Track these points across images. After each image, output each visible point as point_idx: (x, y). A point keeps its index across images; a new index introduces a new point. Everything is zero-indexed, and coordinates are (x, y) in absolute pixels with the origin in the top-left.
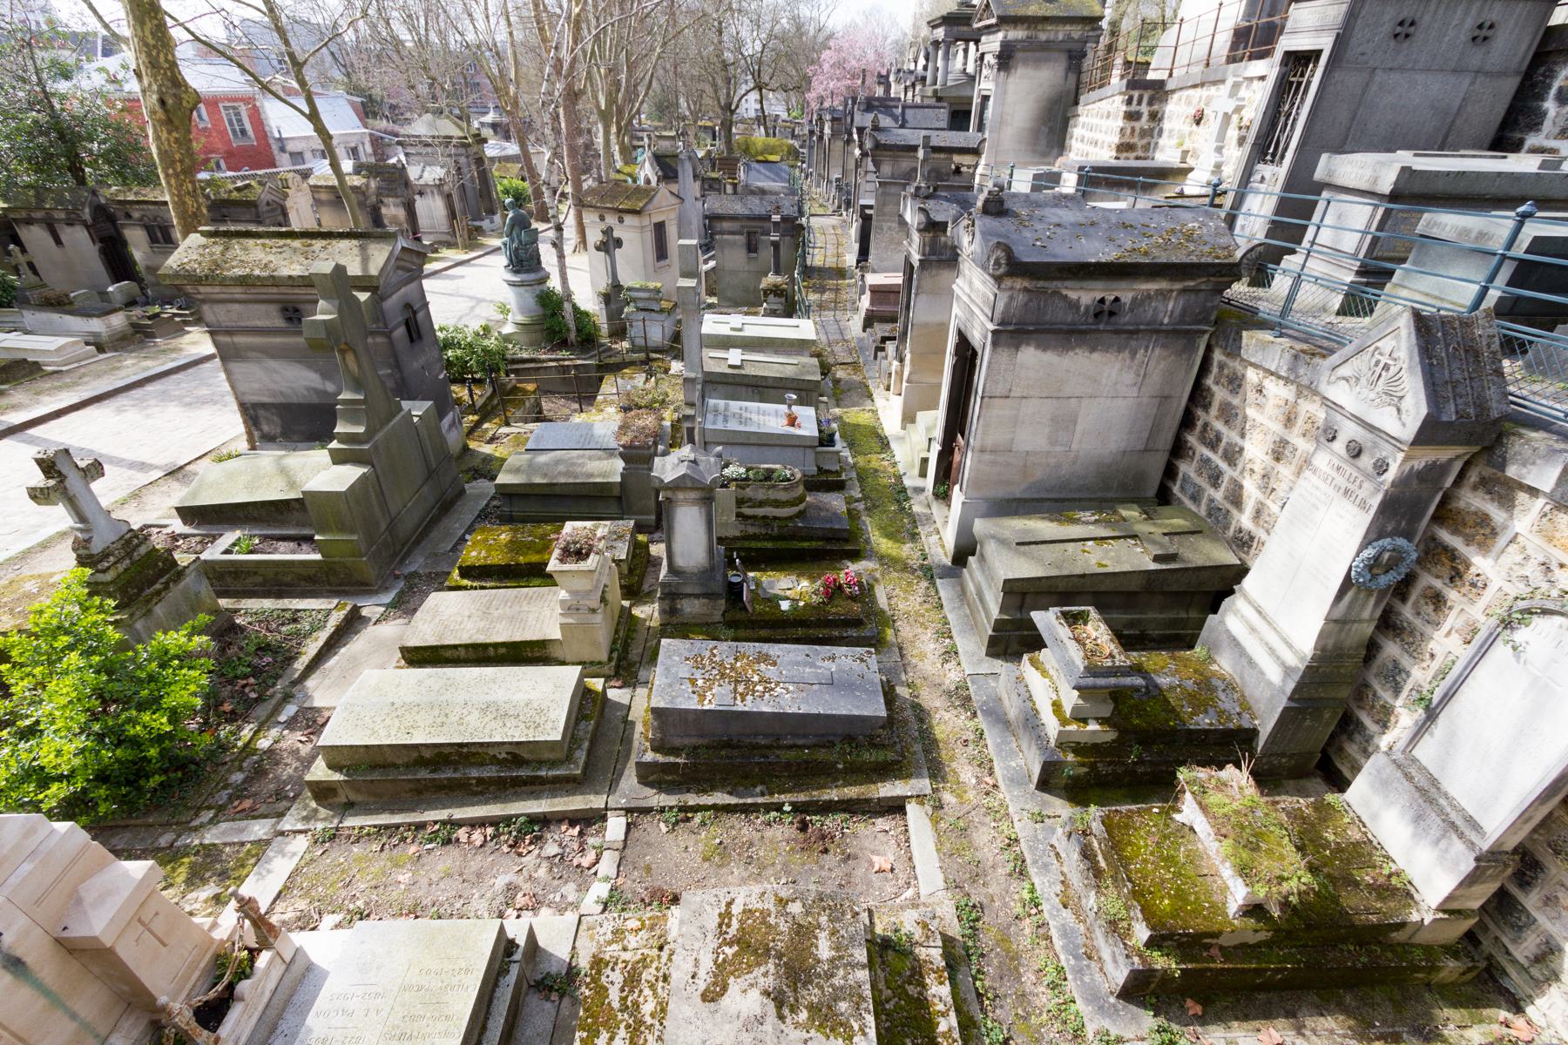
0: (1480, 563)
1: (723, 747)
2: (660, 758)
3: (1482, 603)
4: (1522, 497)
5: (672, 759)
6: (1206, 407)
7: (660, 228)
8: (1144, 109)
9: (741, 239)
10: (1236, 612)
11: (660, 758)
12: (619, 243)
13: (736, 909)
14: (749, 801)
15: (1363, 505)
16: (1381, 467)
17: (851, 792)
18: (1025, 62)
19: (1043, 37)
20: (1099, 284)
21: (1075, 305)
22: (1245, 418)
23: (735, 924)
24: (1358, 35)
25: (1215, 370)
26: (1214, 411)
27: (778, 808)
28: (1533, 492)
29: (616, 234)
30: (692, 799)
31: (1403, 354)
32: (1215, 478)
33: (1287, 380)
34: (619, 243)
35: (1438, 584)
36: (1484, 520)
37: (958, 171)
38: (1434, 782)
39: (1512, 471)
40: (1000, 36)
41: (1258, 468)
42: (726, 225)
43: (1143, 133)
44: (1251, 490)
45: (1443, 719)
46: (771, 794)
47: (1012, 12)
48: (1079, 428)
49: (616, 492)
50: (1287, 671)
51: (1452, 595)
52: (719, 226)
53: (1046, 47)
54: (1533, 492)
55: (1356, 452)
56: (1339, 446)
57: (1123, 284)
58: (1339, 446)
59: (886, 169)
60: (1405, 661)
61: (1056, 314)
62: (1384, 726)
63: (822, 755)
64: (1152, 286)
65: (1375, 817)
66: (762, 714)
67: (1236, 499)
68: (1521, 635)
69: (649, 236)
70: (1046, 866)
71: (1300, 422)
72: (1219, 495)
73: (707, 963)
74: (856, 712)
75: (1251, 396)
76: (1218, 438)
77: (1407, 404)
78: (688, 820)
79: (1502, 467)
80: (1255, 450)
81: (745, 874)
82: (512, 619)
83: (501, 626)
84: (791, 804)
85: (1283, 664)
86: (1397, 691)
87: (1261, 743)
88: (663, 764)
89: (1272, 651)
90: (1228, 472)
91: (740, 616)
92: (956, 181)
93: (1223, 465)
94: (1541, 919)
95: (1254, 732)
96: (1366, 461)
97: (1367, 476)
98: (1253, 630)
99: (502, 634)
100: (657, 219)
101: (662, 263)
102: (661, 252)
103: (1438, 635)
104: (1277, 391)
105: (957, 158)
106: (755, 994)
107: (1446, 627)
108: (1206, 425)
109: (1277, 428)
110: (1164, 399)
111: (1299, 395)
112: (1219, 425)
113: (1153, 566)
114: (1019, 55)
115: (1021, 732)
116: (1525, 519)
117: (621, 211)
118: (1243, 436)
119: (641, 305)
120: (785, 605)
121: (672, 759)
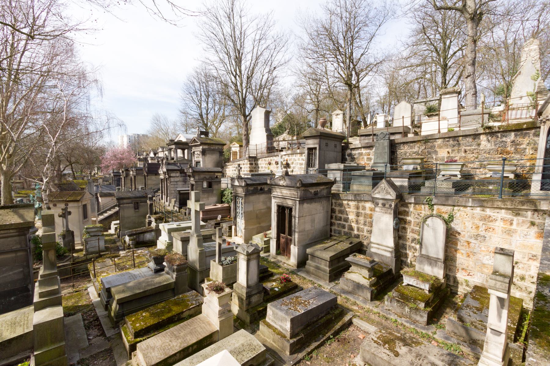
0: (409, 218)
1: (307, 327)
2: (295, 340)
3: (412, 225)
4: (409, 205)
5: (298, 338)
6: (335, 212)
7: (85, 207)
8: (253, 162)
9: (132, 205)
10: (373, 247)
11: (295, 340)
12: (70, 213)
13: (376, 339)
14: (322, 340)
15: (390, 213)
16: (391, 206)
17: (340, 324)
18: (209, 153)
19: (212, 148)
20: (314, 188)
21: (311, 193)
22: (347, 211)
23: (380, 342)
24: (322, 145)
25: (334, 204)
26: (337, 213)
27: (329, 338)
28: (411, 203)
29: (69, 210)
30: (309, 349)
31: (386, 186)
32: (344, 227)
33: (354, 201)
34: (70, 213)
35: (403, 225)
36: (405, 211)
37: (217, 177)
38: (428, 256)
39: (407, 201)
40: (201, 147)
41: (354, 220)
42: (125, 201)
43: (255, 168)
44: (354, 225)
45: (423, 245)
46: (325, 335)
47: (204, 142)
48: (316, 222)
49: (173, 287)
50: (391, 252)
51: (407, 226)
52: (122, 202)
53: (214, 150)
54: (411, 203)
55: (384, 205)
56: (380, 205)
57: (318, 187)
58: (380, 205)
59: (197, 177)
60: (404, 243)
61: (309, 195)
62: (407, 258)
63: (329, 317)
64: (322, 187)
65: (423, 270)
66: (314, 308)
67: (351, 228)
68: (427, 223)
69: (81, 210)
70: (389, 313)
71: (361, 207)
72: (346, 230)
73: (388, 352)
74: (324, 301)
75: (346, 206)
76: (341, 218)
77: (391, 193)
78: (311, 357)
79: (404, 201)
80: (352, 217)
81: (341, 359)
82: (191, 333)
83: (189, 337)
84: (332, 335)
85: (389, 251)
86: (406, 249)
87: (394, 271)
88: (297, 341)
89: (386, 250)
90: (347, 224)
91: (268, 297)
92: (217, 180)
93: (344, 223)
94: (450, 274)
95: (391, 270)
96: (387, 206)
97: (388, 208)
98: (378, 249)
99: (193, 340)
100: (84, 203)
101: (86, 220)
102: (85, 216)
103: (408, 234)
104: (352, 204)
105: (216, 174)
106: (403, 348)
107: (408, 232)
108: (336, 217)
109: (355, 210)
110: (327, 212)
111: (358, 202)
112: (340, 215)
113: (350, 246)
114: (207, 152)
115: (357, 291)
116: (411, 208)
117: (66, 201)
118: (347, 215)
119: (92, 234)
120: (277, 289)
121: (298, 338)
